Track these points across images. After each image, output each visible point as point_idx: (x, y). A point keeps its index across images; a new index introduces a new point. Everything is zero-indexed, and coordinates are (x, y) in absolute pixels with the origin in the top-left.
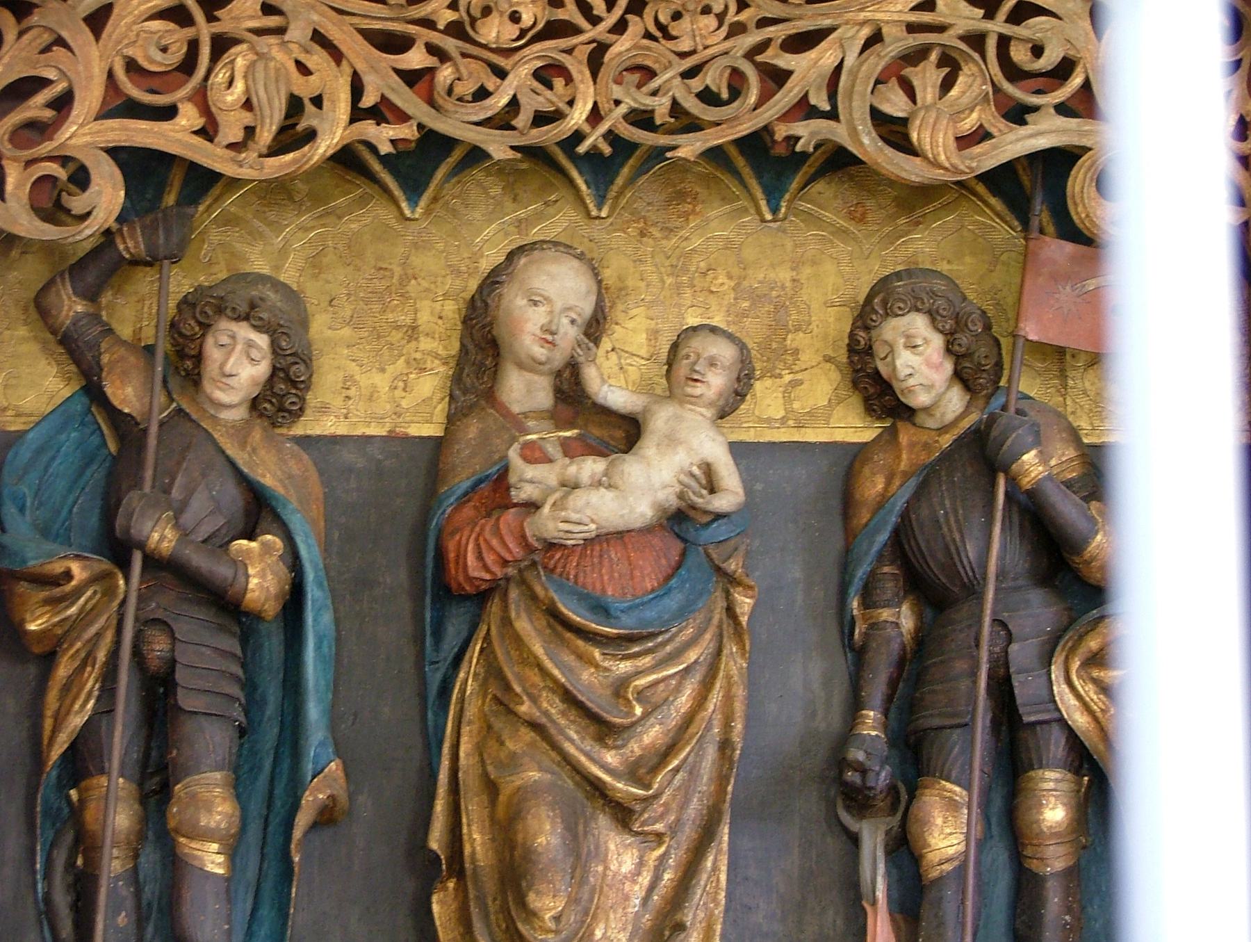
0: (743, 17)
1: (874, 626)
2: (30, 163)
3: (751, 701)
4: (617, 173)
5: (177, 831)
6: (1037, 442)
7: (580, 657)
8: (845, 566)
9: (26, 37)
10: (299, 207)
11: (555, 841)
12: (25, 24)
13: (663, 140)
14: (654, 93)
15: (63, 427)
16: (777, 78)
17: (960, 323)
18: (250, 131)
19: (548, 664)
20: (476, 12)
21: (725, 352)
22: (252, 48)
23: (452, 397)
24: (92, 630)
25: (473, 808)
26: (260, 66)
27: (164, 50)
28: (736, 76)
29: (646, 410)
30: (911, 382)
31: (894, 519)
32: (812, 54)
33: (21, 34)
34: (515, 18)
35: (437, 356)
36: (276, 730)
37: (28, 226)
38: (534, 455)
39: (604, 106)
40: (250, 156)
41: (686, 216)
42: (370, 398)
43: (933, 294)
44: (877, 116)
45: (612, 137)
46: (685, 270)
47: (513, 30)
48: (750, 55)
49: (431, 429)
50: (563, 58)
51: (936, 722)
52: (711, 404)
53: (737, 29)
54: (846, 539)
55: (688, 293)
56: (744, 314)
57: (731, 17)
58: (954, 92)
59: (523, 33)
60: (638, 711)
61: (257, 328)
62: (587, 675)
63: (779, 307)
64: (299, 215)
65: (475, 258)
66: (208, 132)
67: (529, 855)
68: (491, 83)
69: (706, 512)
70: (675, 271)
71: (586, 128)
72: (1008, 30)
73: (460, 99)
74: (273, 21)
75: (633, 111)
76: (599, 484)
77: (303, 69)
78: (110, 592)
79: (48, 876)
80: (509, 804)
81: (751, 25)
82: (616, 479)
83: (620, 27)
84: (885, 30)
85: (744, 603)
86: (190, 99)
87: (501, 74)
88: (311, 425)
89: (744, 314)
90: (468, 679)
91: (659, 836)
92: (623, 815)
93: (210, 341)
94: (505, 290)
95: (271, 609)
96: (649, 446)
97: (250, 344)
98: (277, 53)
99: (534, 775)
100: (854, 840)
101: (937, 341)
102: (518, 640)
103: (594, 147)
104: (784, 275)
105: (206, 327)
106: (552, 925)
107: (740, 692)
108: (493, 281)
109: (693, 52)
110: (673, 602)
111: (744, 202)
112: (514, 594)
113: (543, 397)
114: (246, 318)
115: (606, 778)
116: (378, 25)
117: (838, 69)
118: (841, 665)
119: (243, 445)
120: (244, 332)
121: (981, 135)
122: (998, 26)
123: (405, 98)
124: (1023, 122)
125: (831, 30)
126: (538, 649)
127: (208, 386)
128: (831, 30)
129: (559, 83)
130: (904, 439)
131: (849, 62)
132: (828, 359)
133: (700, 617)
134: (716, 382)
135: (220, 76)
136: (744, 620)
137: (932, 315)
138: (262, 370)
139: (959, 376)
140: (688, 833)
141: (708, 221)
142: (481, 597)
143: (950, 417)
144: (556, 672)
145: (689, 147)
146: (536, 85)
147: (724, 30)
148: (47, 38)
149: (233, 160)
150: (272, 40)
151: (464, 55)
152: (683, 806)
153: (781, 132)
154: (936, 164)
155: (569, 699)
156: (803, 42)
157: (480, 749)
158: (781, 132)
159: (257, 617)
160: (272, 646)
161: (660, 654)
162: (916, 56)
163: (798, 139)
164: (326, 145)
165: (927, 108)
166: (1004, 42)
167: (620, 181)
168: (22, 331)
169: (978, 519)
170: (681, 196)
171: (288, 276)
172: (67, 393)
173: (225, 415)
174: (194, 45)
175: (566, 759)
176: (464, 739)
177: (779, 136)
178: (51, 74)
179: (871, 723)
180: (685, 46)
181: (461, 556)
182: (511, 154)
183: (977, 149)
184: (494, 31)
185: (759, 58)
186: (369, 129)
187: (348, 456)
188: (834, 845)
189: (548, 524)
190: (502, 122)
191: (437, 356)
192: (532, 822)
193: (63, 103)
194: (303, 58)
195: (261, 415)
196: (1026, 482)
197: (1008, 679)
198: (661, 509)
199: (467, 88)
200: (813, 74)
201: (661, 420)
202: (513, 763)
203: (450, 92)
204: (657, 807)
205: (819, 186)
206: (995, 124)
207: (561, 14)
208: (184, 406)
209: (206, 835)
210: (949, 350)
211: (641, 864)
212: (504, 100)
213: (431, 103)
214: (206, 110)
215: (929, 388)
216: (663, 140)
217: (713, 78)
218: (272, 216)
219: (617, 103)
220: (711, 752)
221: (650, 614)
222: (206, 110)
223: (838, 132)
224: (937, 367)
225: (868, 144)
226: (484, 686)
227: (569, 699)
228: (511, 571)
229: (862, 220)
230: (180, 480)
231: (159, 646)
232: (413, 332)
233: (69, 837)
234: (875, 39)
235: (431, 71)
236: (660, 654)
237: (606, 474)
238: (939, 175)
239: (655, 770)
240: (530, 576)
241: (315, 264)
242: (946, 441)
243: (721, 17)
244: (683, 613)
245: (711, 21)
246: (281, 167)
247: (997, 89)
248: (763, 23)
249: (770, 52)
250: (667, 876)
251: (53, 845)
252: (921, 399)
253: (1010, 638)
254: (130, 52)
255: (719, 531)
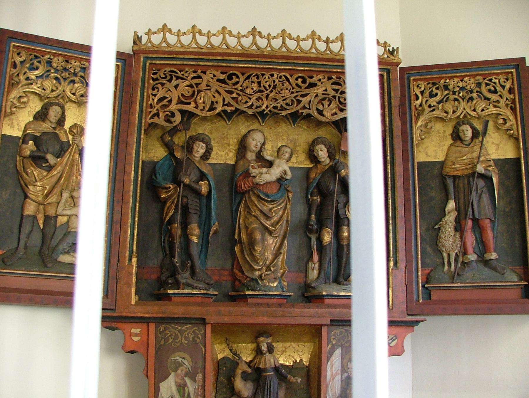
0: (293, 91)
1: (313, 200)
2: (164, 112)
3: (292, 213)
4: (266, 117)
5: (189, 234)
6: (344, 168)
7: (263, 204)
8: (308, 189)
9: (163, 89)
10: (208, 121)
11: (260, 237)
12: (163, 87)
13: (279, 112)
14: (278, 103)
15: (166, 160)
16: (299, 102)
17: (330, 147)
18: (204, 107)
19: (258, 206)
20: (245, 88)
21: (289, 150)
22: (205, 92)
23: (237, 157)
24: (174, 198)
25: (243, 231)
26: (206, 96)
27: (188, 92)
28: (292, 101)
29: (274, 160)
30: (321, 157)
31: (317, 181)
32: (306, 98)
33: (162, 89)
34: (252, 89)
35: (233, 149)
36: (205, 216)
37: (164, 123)
38: (253, 168)
39: (269, 105)
40: (204, 112)
41: (278, 125)
42: (221, 156)
43: (325, 141)
44: (318, 110)
45: (270, 111)
46: (278, 135)
47: (252, 91)
48: (295, 97)
49: (232, 162)
50: (261, 96)
51: (325, 217)
52: (286, 160)
53: (292, 93)
54: (307, 185)
55: (279, 140)
56: (289, 143)
57: (291, 91)
58: (331, 106)
59: (254, 92)
60: (274, 214)
61: (203, 143)
62: (265, 208)
63: (295, 143)
64: (208, 123)
65: (240, 132)
66: (197, 107)
67: (255, 240)
68: (248, 100)
69: (284, 178)
70: (276, 135)
71: (266, 109)
72: (340, 96)
73: (243, 103)
74: (208, 88)
75: (274, 106)
76: (266, 173)
77: (214, 97)
78: (176, 191)
79: (164, 242)
80: (251, 230)
81: (295, 92)
82: (270, 172)
83: (271, 91)
84: (319, 94)
85: (291, 195)
86: (193, 101)
87: (250, 99)
88: (210, 161)
89: (289, 143)
90: (242, 208)
91: (276, 237)
92: (270, 233)
93: (195, 145)
94: (248, 137)
95: (206, 194)
96: (275, 167)
97: (202, 146)
98: (209, 94)
99: (255, 225)
100: (310, 239)
101: (326, 150)
102: (252, 201)
103: (267, 113)
104: (296, 137)
105: (194, 143)
106: (259, 252)
107: (289, 211)
108: (245, 136)
109: (284, 97)
110: (279, 195)
111: (289, 124)
112: (251, 193)
113: (254, 157)
114: (202, 141)
115: (268, 226)
116: (227, 89)
117: (310, 101)
118: (306, 207)
119: (200, 164)
120: (201, 144)
121: (336, 114)
122: (338, 95)
123: (233, 102)
124: (343, 112)
125: (309, 94)
126: (256, 203)
127: (194, 154)
128: (309, 94)
129: (260, 101)
130: (318, 167)
131: (312, 100)
132: (304, 152)
133: (284, 198)
134: (287, 156)
135: (199, 97)
136: (290, 198)
137: (325, 145)
138: (204, 151)
139: (329, 156)
140: (281, 237)
141: (282, 127)
142: (244, 193)
143: (327, 163)
144: (259, 207)
145: (284, 113)
146: (256, 101)
147: (290, 93)
148: (167, 90)
149: (201, 113)
150: (208, 91)
151: (243, 95)
152: (280, 232)
153: (300, 111)
154: (328, 119)
155: (261, 211)
156: (304, 96)
157: (244, 221)
158: (300, 111)
159: (203, 195)
160: (204, 201)
161: (277, 204)
162: (324, 99)
163: (303, 113)
164: (218, 111)
165: (326, 108)
166: (339, 98)
167: (267, 119)
168: (157, 143)
169: (332, 182)
170: (277, 122)
171: (206, 133)
172: (166, 154)
173: (197, 159)
174: (194, 92)
175: (261, 222)
176: (241, 219)
177: (300, 112)
178: (168, 96)
179: (313, 217)
180: (283, 95)
181: (240, 186)
182: (252, 113)
183: (335, 116)
184: (248, 91)
185: (296, 98)
186: (226, 108)
187: (217, 167)
188: (305, 239)
189: (257, 180)
190: (251, 106)
191: (233, 149)
192: (256, 234)
193: (170, 101)
194: (214, 95)
195: (202, 159)
196: (342, 175)
197: (338, 210)
198: (277, 178)
199: (244, 101)
200: (306, 101)
201: (277, 162)
202: (251, 223)
203: (241, 101)
204: (276, 232)
205: (302, 121)
206: (338, 112)
207: (261, 89)
208: (189, 157)
209: (194, 235)
210: (328, 151)
211: (273, 242)
212: (251, 104)
213: (237, 103)
214: (196, 103)
215: (324, 158)
216: (279, 112)
217: (288, 101)
218: (203, 123)
219: (271, 105)
220: (285, 222)
221: (275, 197)
222: (196, 103)
223: (310, 112)
224: (326, 154)
225: (316, 114)
226: (245, 210)
227: (261, 211)
228: (250, 188)
229: (309, 128)
230: (189, 170)
231: (185, 201)
232: (229, 145)
233: (168, 235)
234: (317, 96)
235: (237, 98)
236: (277, 204)
237: (267, 171)
238: (328, 120)
239: (276, 225)
240: (253, 189)
241: (211, 132)
242: (327, 167)
243: (289, 90)
244: (281, 197)
245: (288, 91)
246: (210, 114)
247: (338, 106)
248: (297, 92)
249: (298, 97)
250: (277, 244)
251: (165, 236)
252: (323, 160)
253: (338, 203)
254: (182, 92)
255: (286, 182)
